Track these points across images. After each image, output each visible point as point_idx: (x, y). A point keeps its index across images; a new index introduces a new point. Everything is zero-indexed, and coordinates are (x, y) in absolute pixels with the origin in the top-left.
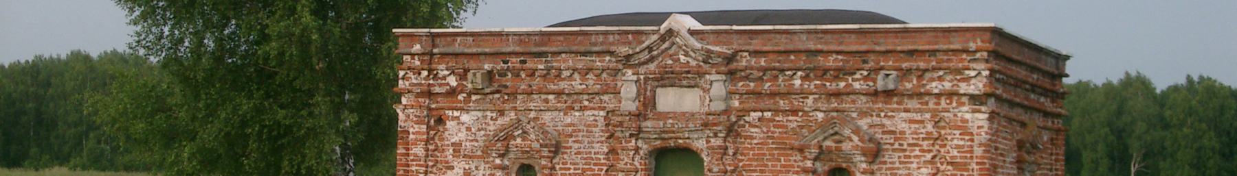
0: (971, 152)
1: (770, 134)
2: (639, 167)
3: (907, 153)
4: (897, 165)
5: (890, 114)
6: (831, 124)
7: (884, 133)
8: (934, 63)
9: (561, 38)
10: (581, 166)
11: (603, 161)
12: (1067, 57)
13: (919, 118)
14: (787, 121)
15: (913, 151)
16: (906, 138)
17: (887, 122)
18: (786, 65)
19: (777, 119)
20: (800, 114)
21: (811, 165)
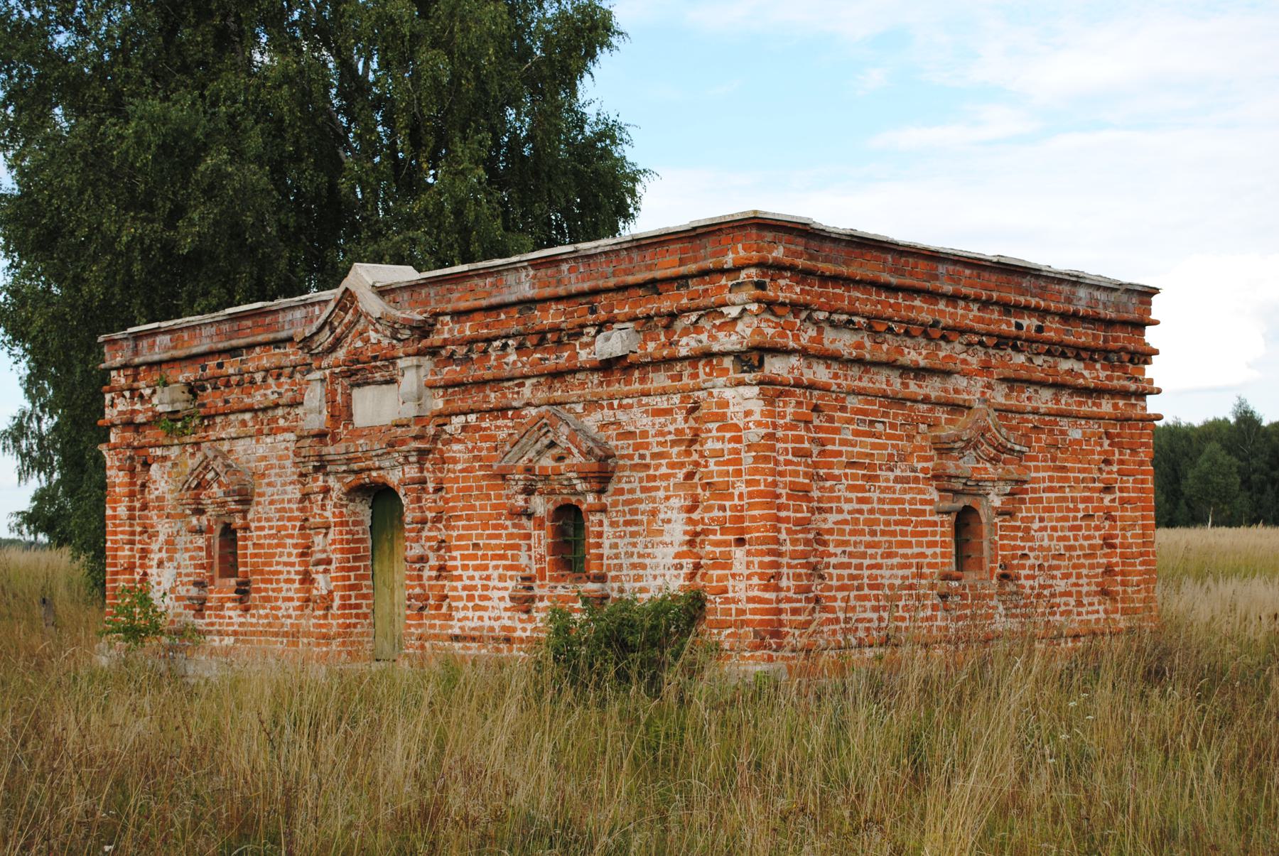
0: (738, 462)
1: (476, 453)
2: (332, 520)
3: (651, 472)
4: (638, 495)
5: (625, 401)
6: (540, 429)
7: (621, 436)
8: (685, 301)
9: (249, 323)
10: (274, 523)
11: (297, 514)
12: (1153, 292)
13: (665, 406)
14: (497, 427)
15: (657, 467)
16: (648, 444)
17: (622, 416)
18: (494, 332)
19: (484, 425)
20: (510, 413)
21: (522, 503)
